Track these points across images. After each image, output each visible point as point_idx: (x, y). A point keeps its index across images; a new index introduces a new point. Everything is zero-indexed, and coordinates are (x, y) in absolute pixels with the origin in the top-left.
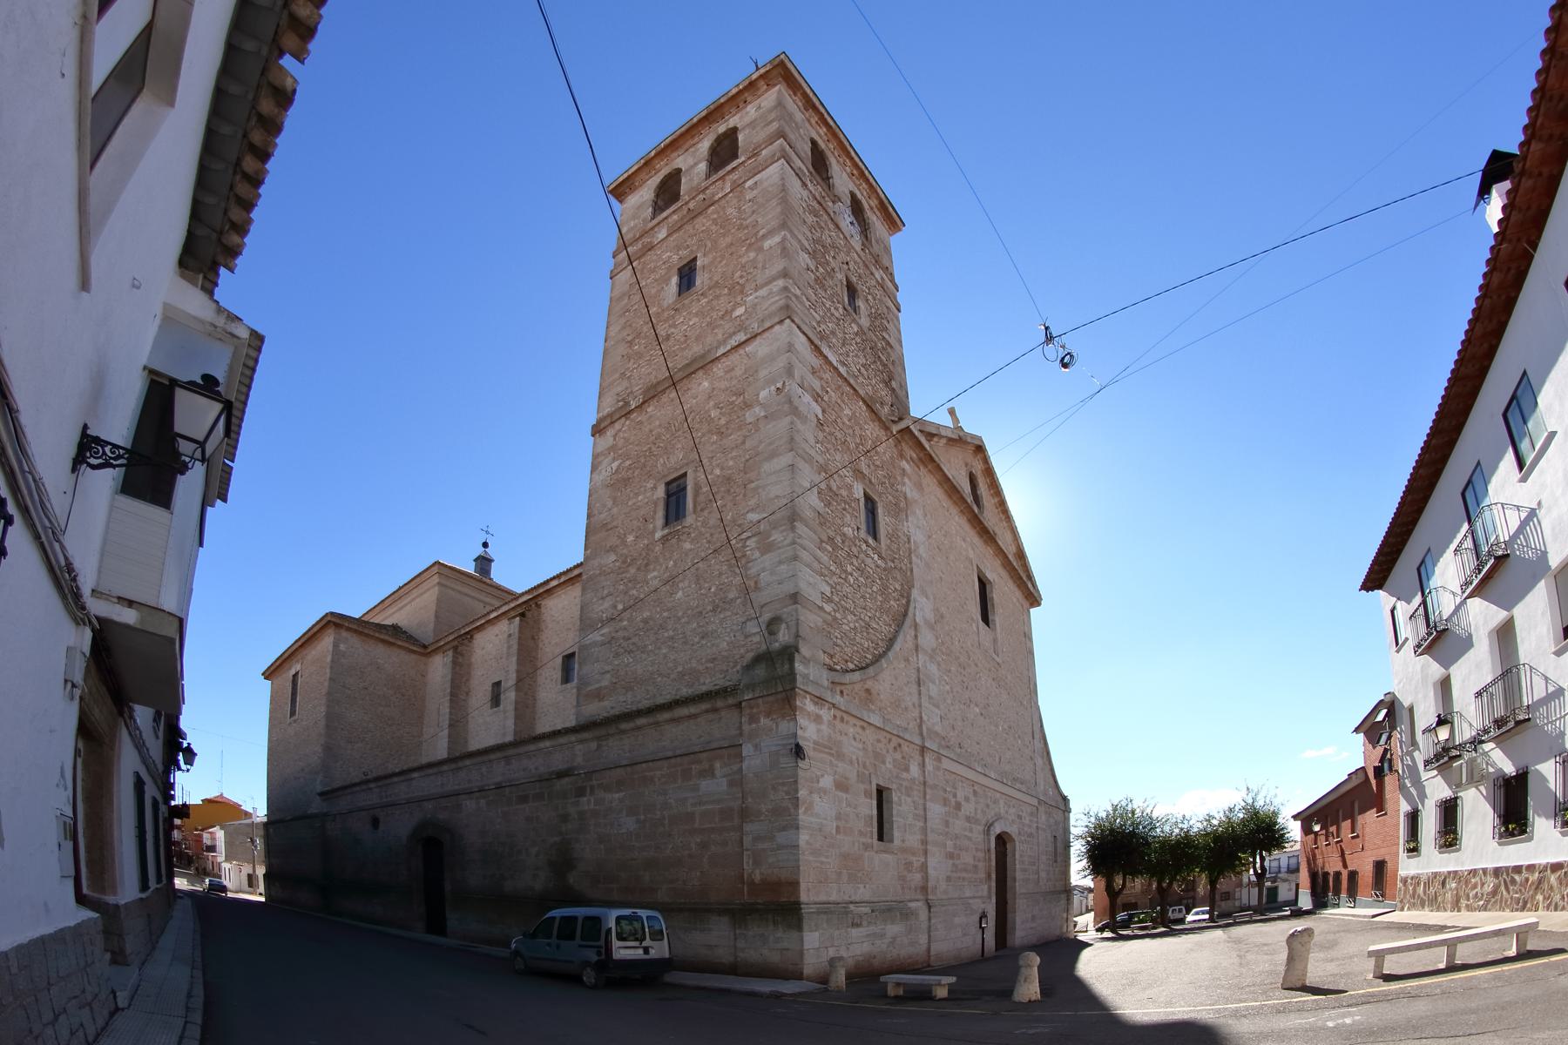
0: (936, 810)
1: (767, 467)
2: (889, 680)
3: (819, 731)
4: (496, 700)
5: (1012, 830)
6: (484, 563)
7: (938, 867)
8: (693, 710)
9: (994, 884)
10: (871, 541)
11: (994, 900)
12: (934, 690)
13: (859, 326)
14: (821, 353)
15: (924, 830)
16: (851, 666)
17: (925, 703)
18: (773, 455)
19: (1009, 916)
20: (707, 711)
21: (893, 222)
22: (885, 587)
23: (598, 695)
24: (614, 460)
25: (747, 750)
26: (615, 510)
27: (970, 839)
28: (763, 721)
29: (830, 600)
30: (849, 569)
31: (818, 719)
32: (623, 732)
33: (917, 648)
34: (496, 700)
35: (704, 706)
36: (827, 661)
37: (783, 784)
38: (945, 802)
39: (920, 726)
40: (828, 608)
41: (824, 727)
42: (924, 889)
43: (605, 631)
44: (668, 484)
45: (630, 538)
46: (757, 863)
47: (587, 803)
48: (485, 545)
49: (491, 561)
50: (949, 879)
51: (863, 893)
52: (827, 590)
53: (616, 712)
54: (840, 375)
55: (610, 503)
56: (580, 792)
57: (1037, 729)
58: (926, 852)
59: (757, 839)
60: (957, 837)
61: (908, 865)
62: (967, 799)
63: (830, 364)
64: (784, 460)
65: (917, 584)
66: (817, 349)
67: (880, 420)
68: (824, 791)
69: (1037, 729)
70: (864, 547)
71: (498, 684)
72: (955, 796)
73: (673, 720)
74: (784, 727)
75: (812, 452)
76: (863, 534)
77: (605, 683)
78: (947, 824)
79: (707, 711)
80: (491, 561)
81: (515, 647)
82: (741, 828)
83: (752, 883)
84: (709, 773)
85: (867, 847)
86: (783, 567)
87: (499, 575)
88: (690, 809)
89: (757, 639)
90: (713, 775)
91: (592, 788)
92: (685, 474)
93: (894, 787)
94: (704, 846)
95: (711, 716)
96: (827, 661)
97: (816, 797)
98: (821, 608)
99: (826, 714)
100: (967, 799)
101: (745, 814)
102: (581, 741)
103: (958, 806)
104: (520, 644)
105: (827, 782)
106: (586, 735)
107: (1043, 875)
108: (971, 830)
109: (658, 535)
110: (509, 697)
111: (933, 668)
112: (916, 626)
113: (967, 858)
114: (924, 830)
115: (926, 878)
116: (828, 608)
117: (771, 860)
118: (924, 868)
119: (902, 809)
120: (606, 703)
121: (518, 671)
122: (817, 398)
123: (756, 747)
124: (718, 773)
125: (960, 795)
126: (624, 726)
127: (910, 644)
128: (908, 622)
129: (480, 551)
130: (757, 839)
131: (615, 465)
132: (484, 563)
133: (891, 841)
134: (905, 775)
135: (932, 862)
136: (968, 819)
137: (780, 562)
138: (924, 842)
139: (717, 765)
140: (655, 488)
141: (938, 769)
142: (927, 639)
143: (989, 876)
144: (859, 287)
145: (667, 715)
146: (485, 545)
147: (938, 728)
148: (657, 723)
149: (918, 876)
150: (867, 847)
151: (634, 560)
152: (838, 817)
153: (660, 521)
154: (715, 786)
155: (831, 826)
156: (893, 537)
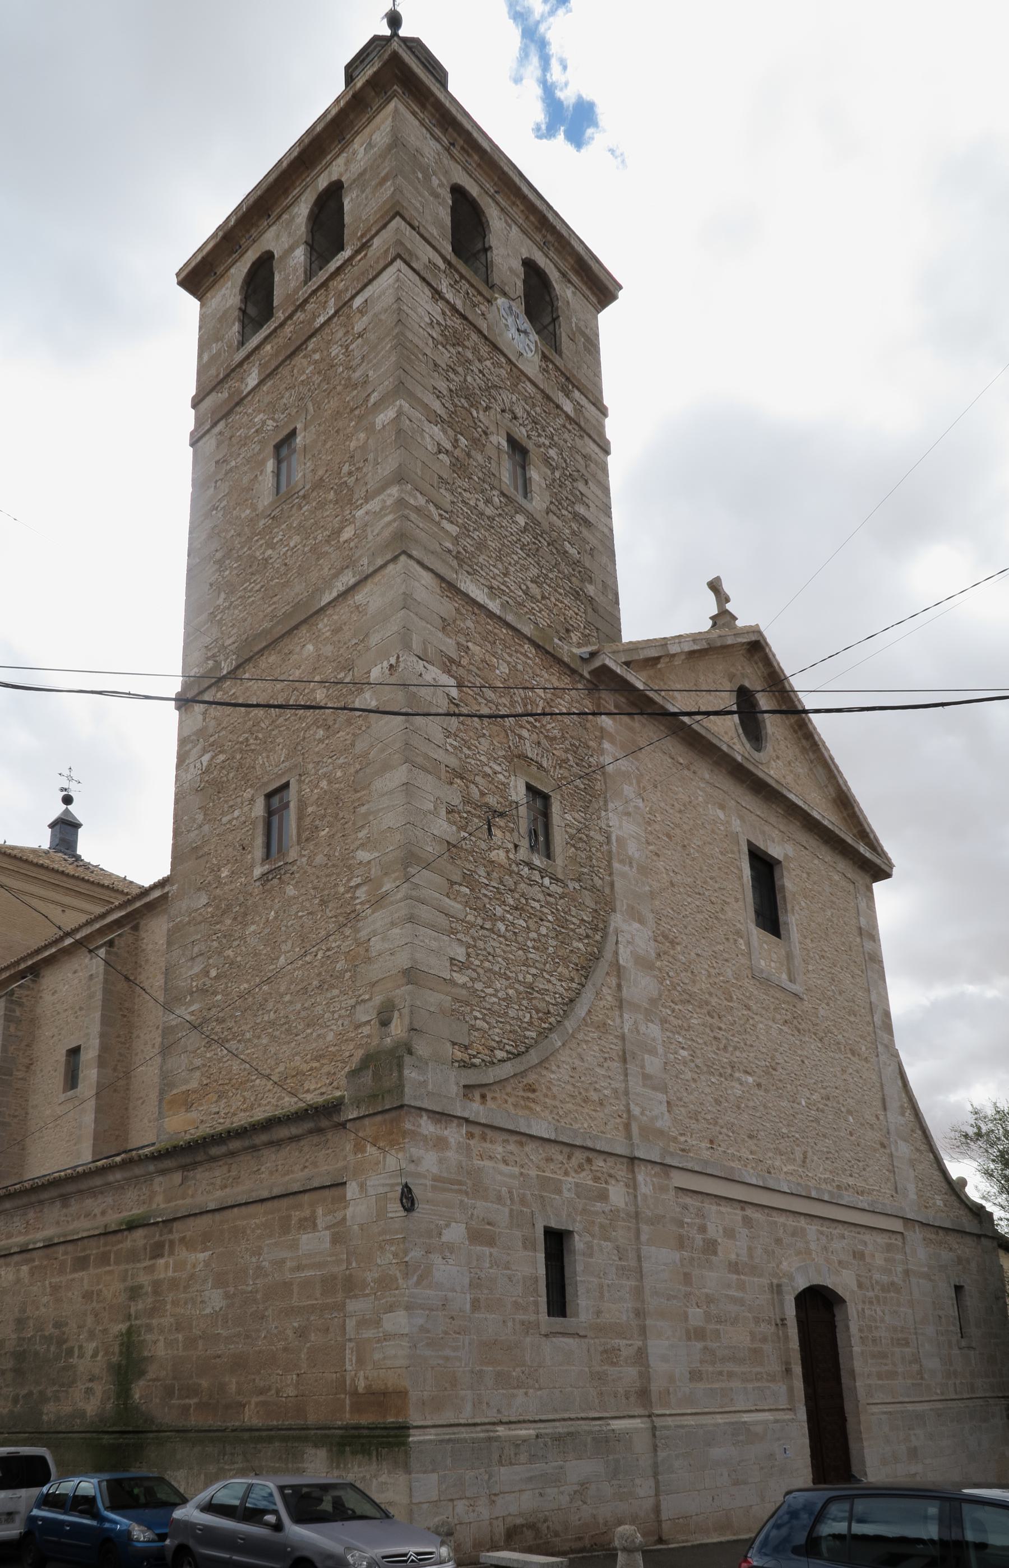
0: (661, 1259)
1: (380, 784)
2: (577, 1063)
3: (441, 1161)
4: (72, 1079)
5: (842, 1281)
6: (66, 829)
7: (668, 1355)
8: (294, 1130)
9: (799, 1384)
10: (537, 861)
11: (802, 1414)
12: (653, 1064)
13: (529, 515)
14: (458, 591)
15: (638, 1292)
16: (500, 1054)
17: (635, 1085)
18: (386, 767)
19: (853, 1446)
20: (311, 1132)
21: (602, 289)
22: (562, 922)
23: (186, 1101)
24: (204, 751)
25: (352, 1190)
26: (206, 828)
27: (741, 1302)
28: (370, 1149)
29: (464, 967)
30: (499, 911)
31: (440, 1144)
32: (214, 1159)
33: (620, 1004)
34: (72, 1079)
35: (309, 1125)
36: (459, 1055)
37: (391, 1242)
38: (681, 1243)
39: (627, 1127)
40: (461, 979)
41: (451, 1154)
42: (644, 1394)
43: (195, 1007)
44: (269, 796)
45: (225, 873)
46: (361, 1362)
47: (165, 1268)
48: (68, 800)
49: (77, 826)
50: (695, 1376)
51: (524, 1403)
52: (460, 953)
53: (205, 1130)
54: (491, 615)
55: (200, 817)
56: (157, 1251)
57: (893, 1090)
58: (643, 1331)
59: (363, 1323)
60: (710, 1300)
61: (610, 1355)
62: (730, 1233)
63: (474, 602)
64: (400, 774)
65: (622, 904)
66: (451, 588)
67: (559, 661)
68: (451, 1248)
69: (893, 1090)
70: (525, 871)
71: (74, 1052)
72: (703, 1229)
73: (271, 1144)
74: (392, 1161)
75: (439, 755)
76: (523, 853)
77: (194, 1085)
78: (687, 1278)
79: (311, 1132)
80: (77, 826)
81: (99, 996)
82: (341, 1307)
83: (355, 1393)
84: (309, 1224)
85: (528, 1327)
86: (396, 931)
87: (90, 848)
88: (288, 1276)
89: (366, 1030)
90: (315, 1226)
91: (172, 1243)
92: (286, 786)
93: (577, 1227)
94: (302, 1333)
95: (316, 1139)
96: (459, 1055)
97: (436, 1259)
98: (452, 982)
99: (454, 1134)
100: (730, 1233)
101: (351, 1286)
102: (163, 1172)
103: (711, 1247)
104: (106, 991)
105: (455, 1233)
106: (168, 1163)
107: (932, 1364)
108: (741, 1286)
109: (258, 872)
110: (90, 1075)
111: (654, 1030)
112: (618, 969)
113: (738, 1337)
114: (638, 1292)
115: (645, 1376)
116: (461, 979)
117: (377, 1356)
118: (641, 1356)
119: (590, 1266)
120: (193, 1115)
121: (102, 1035)
122: (448, 665)
123: (362, 1186)
124: (321, 1223)
125: (714, 1231)
126: (214, 1151)
127: (609, 997)
128: (603, 966)
129: (58, 809)
130: (363, 1323)
131: (206, 759)
132: (66, 829)
133: (576, 1315)
134: (599, 1206)
135: (656, 1347)
136: (734, 1267)
137: (393, 924)
138: (639, 1313)
139: (320, 1211)
140: (252, 800)
141: (663, 1189)
142: (641, 986)
143: (788, 1371)
144: (530, 446)
145: (264, 1138)
146: (68, 800)
147: (664, 1123)
148: (254, 1148)
149: (632, 1372)
150: (528, 1327)
151: (229, 907)
152: (475, 1284)
153: (259, 853)
154: (314, 1243)
155: (463, 1301)
156: (578, 838)
